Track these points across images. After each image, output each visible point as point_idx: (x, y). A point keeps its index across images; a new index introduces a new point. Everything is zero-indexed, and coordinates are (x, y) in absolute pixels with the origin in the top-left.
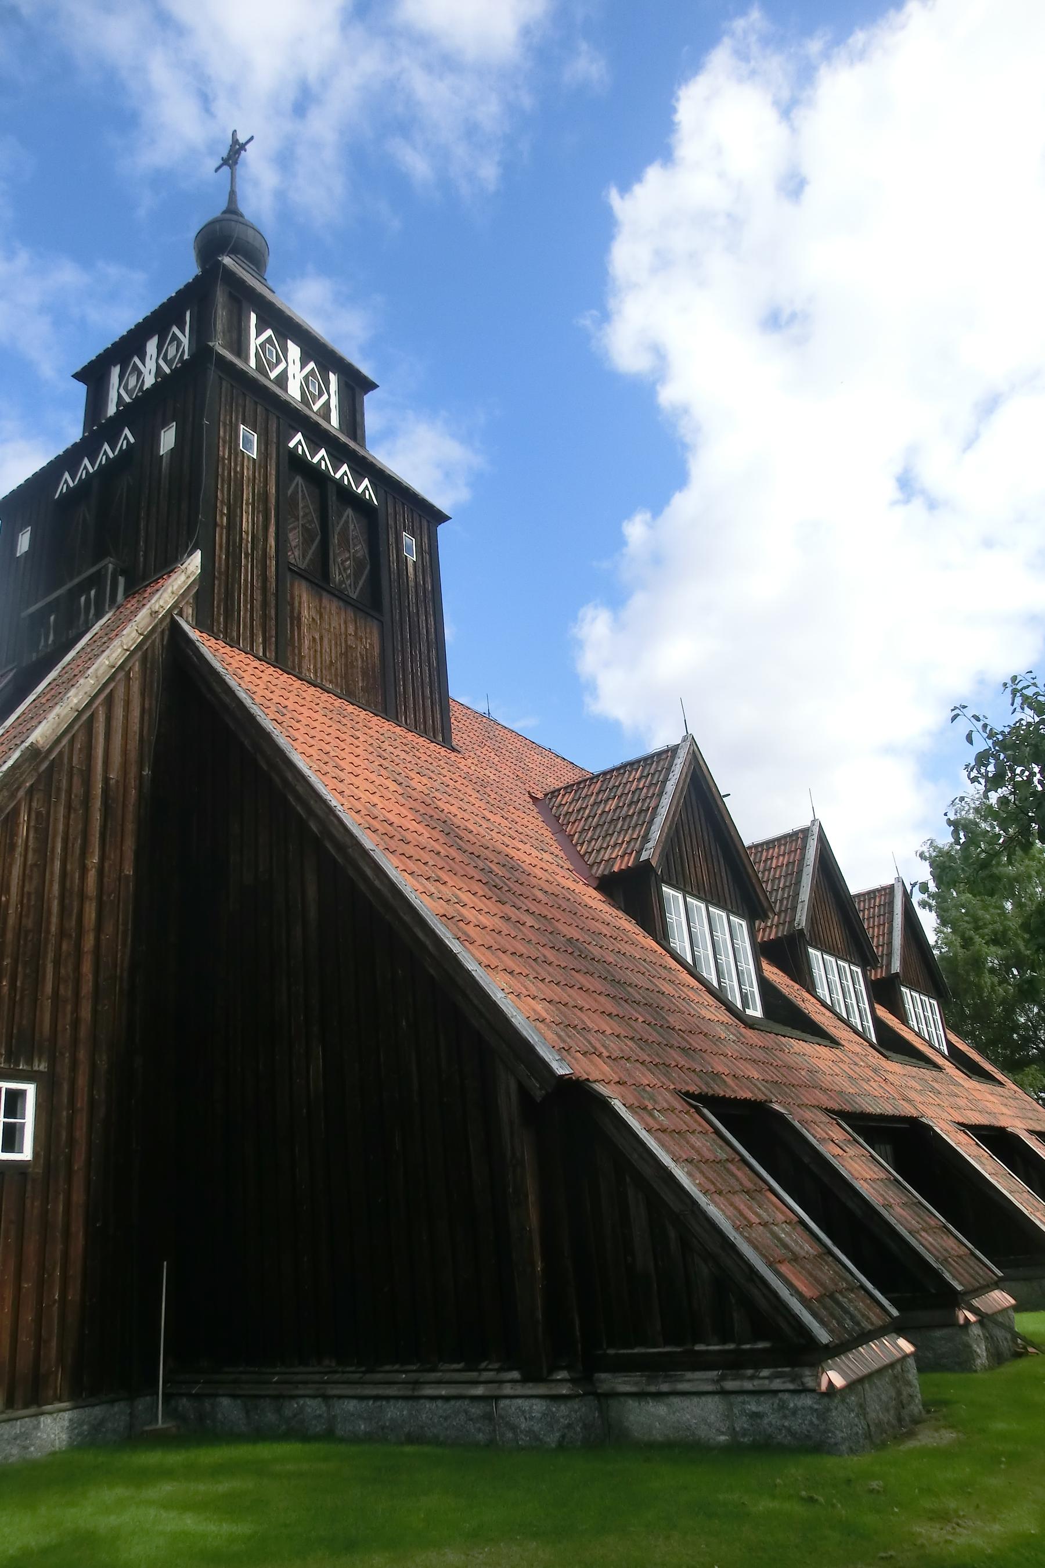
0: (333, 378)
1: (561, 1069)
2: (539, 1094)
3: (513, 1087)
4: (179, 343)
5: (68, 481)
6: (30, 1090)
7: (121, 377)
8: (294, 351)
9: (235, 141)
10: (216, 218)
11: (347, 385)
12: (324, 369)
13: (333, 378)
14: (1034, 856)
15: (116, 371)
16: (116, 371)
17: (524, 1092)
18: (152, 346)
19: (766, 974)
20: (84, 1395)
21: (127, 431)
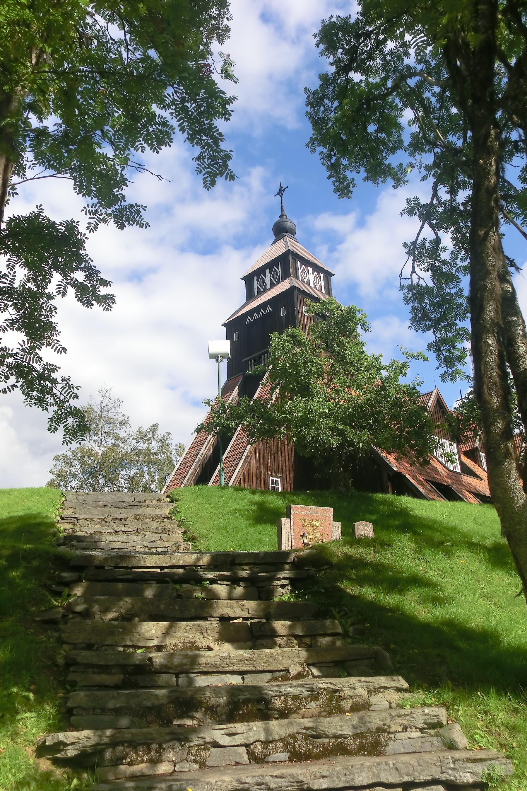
0: (322, 275)
1: (395, 469)
2: (391, 475)
3: (386, 474)
4: (277, 273)
5: (249, 319)
6: (279, 480)
7: (258, 280)
8: (310, 270)
9: (281, 187)
10: (435, 522)
11: (326, 276)
12: (319, 273)
13: (322, 275)
14: (117, 478)
15: (255, 278)
16: (255, 278)
17: (389, 475)
18: (268, 272)
19: (462, 460)
20: (515, 318)
21: (269, 306)
